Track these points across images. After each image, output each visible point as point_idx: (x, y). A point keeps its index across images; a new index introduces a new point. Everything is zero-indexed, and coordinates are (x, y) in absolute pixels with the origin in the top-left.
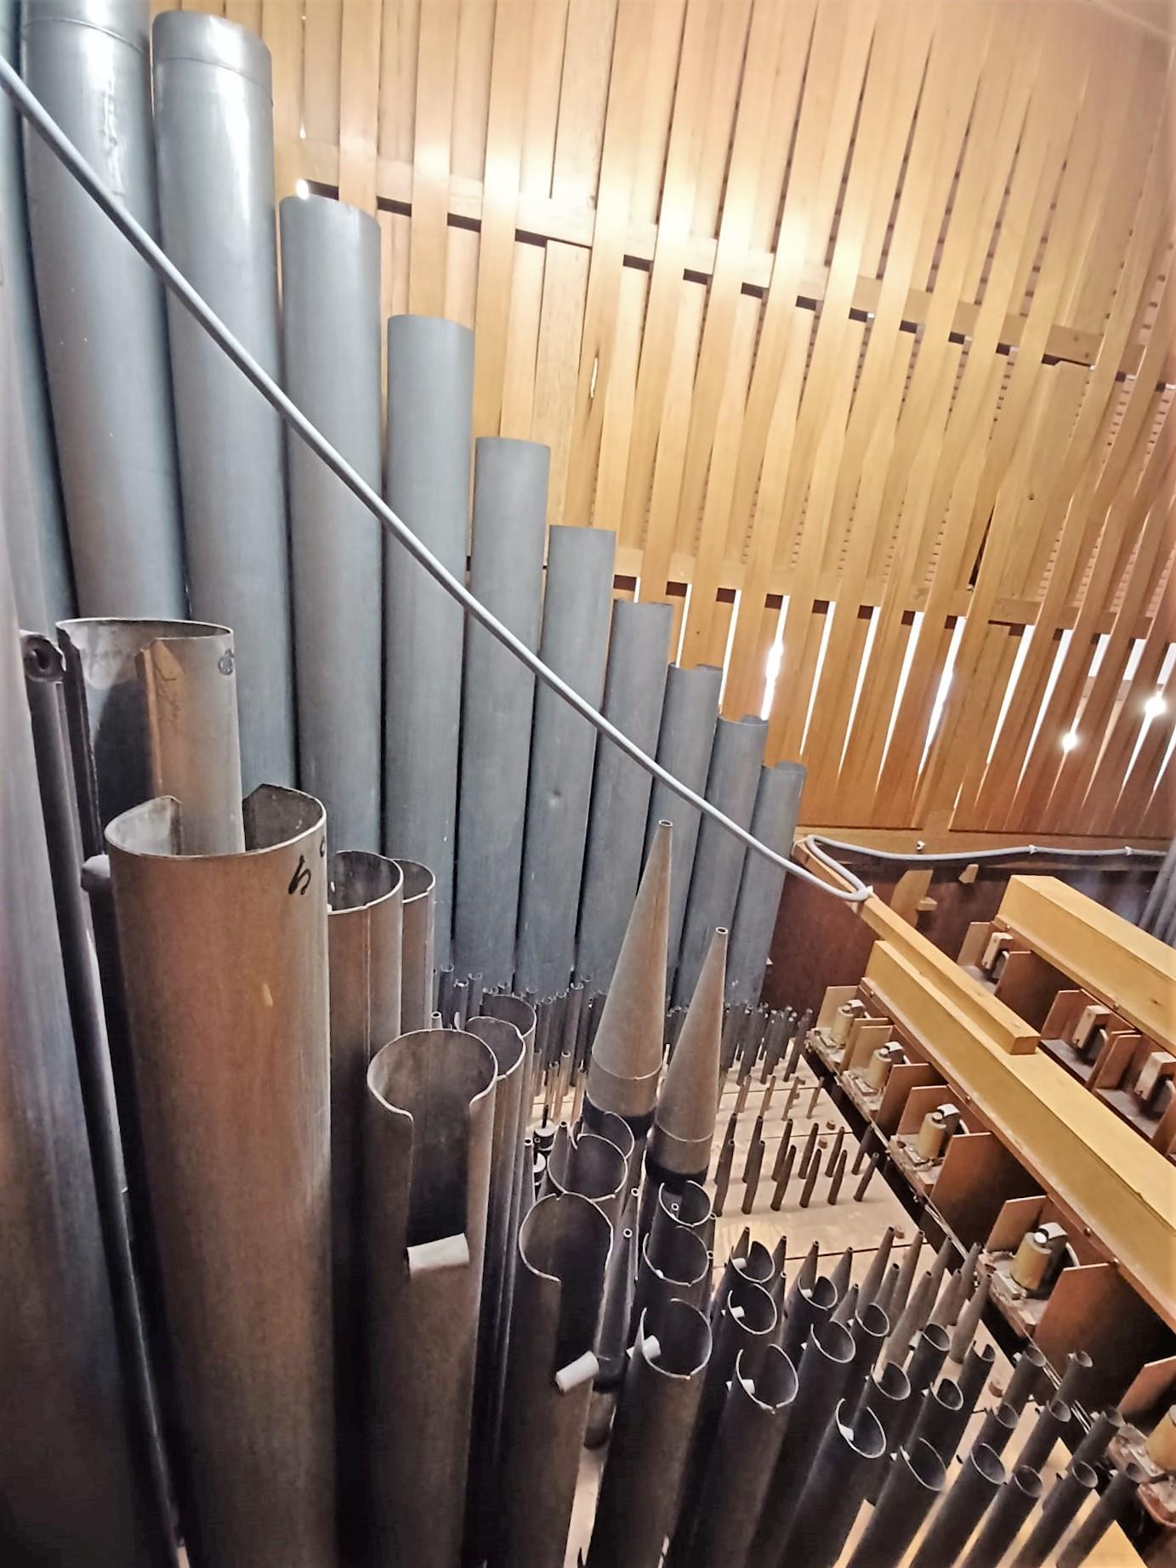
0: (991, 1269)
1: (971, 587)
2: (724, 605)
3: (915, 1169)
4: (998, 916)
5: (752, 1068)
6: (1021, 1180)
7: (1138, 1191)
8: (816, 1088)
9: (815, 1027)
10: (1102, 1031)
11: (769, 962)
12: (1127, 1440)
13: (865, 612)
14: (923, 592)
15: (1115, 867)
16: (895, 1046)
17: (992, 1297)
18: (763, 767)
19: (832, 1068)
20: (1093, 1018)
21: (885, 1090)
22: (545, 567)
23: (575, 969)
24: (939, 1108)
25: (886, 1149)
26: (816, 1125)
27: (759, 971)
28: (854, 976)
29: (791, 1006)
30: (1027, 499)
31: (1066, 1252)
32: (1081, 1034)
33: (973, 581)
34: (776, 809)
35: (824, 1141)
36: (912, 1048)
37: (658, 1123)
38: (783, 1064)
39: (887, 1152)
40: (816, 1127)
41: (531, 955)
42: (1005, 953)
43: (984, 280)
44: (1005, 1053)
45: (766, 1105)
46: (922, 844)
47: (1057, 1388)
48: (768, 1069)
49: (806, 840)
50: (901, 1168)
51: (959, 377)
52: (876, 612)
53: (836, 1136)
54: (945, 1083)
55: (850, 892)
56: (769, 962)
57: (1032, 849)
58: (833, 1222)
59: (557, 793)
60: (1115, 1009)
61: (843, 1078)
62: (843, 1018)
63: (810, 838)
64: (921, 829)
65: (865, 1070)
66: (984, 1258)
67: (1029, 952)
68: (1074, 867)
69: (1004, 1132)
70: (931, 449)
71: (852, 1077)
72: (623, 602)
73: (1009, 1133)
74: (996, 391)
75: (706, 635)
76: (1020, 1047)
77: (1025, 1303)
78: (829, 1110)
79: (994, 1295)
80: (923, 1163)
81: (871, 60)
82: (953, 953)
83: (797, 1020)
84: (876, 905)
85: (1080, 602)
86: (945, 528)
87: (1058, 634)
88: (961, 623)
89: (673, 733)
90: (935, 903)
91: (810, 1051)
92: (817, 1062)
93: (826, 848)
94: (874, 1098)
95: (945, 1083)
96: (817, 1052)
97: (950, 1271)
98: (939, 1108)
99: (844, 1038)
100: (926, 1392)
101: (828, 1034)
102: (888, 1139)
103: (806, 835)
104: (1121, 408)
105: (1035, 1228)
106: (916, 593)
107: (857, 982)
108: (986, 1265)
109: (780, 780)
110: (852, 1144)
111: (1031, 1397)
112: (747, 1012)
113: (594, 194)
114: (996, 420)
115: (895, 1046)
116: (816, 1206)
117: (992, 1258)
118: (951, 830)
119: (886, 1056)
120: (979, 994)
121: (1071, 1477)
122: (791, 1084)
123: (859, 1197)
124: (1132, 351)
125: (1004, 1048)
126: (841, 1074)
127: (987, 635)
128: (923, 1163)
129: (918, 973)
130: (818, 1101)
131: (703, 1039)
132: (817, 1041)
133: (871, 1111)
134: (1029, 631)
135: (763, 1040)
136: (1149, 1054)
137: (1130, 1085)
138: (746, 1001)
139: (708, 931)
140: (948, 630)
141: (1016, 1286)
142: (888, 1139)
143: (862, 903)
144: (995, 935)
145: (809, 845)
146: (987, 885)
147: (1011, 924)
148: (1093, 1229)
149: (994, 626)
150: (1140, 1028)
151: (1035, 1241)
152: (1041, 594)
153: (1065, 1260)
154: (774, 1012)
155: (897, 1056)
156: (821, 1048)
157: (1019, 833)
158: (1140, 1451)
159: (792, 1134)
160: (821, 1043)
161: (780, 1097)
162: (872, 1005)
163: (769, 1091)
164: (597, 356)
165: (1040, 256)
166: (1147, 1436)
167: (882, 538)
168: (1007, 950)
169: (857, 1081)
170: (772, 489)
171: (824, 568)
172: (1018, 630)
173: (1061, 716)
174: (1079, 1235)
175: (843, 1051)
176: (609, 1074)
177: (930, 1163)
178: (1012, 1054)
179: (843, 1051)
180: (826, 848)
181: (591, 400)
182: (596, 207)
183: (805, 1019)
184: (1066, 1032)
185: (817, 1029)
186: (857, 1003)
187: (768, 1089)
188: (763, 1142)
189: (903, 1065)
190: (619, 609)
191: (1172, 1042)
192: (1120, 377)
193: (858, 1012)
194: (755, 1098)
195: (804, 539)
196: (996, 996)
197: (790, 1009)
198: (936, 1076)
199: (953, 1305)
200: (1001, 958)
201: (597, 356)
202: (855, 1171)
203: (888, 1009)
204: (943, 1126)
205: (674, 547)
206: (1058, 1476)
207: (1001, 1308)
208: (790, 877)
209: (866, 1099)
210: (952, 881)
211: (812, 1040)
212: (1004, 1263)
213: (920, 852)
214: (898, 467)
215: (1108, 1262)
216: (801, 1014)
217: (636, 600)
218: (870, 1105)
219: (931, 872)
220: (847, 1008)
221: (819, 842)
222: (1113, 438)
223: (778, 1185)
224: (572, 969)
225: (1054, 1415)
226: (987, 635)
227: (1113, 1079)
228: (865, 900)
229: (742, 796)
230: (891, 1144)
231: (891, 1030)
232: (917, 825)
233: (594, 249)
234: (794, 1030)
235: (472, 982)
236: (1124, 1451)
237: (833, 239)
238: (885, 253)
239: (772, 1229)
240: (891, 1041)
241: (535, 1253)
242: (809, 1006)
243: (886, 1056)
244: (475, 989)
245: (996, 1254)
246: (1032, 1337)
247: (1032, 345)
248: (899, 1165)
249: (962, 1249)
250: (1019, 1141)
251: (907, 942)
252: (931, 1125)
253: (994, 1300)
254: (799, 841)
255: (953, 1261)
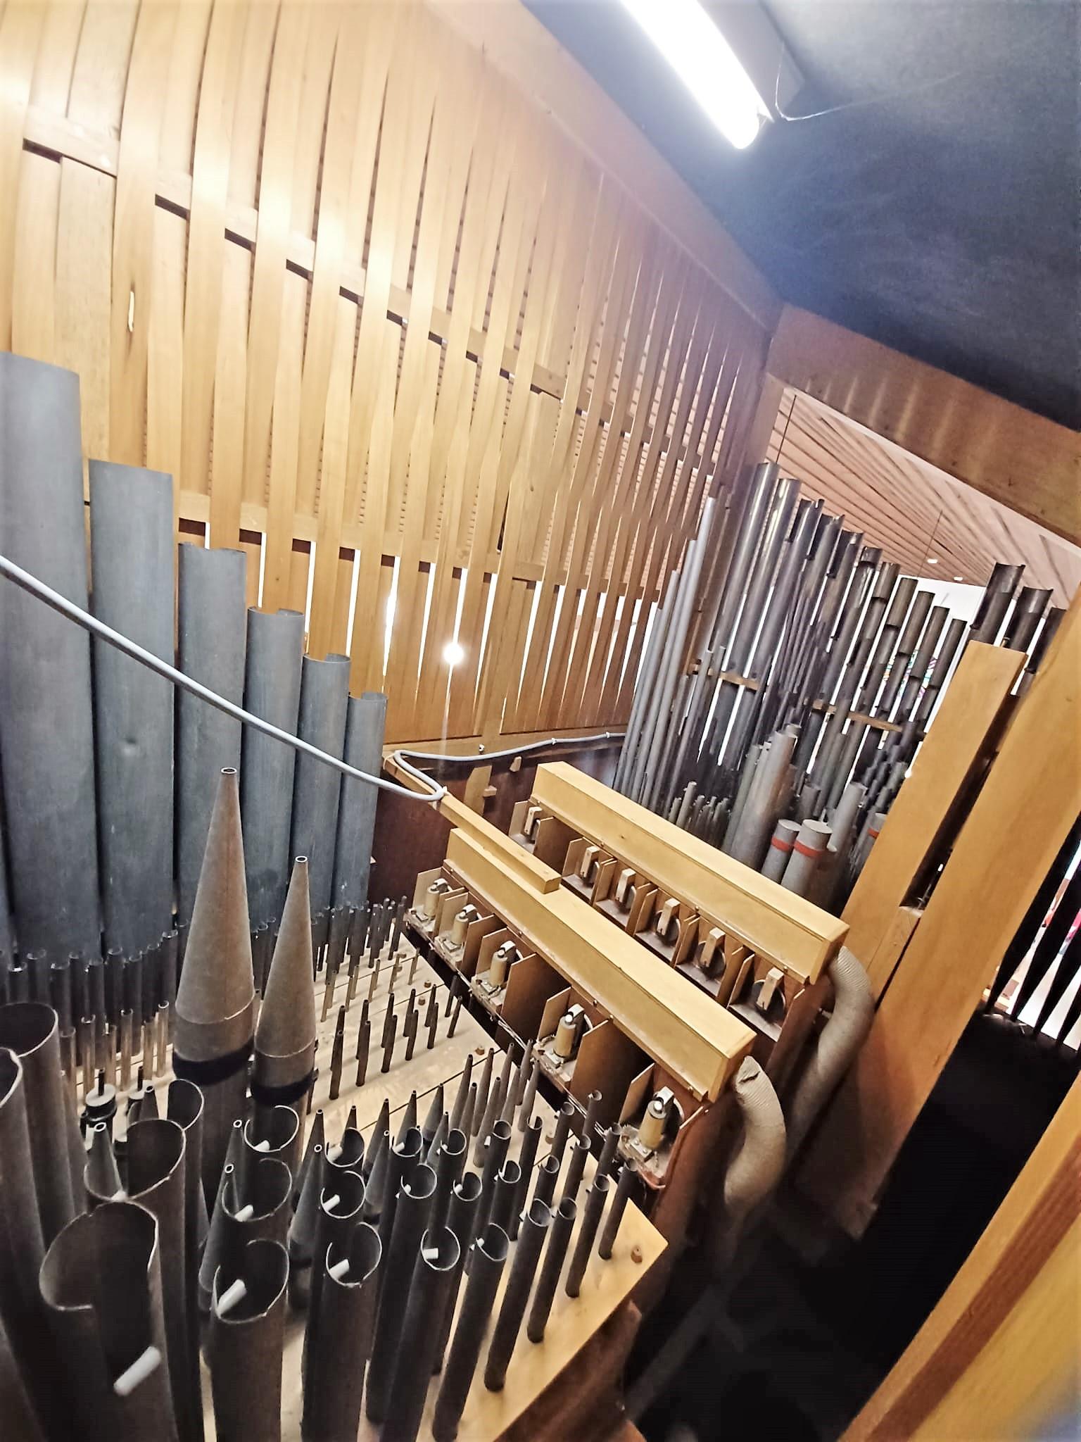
0: (542, 1052)
1: (499, 551)
2: (300, 555)
3: (489, 997)
4: (532, 795)
5: (361, 957)
6: (556, 981)
7: (619, 966)
8: (414, 958)
9: (411, 907)
10: (596, 863)
11: (373, 861)
12: (628, 1138)
13: (424, 567)
14: (466, 553)
15: (601, 747)
16: (470, 908)
17: (543, 1071)
18: (349, 697)
19: (426, 937)
20: (591, 855)
21: (465, 943)
22: (87, 503)
23: (179, 910)
24: (502, 947)
25: (469, 988)
26: (414, 990)
27: (364, 871)
28: (436, 856)
29: (388, 897)
30: (529, 490)
31: (585, 1021)
32: (585, 869)
33: (500, 548)
34: (364, 732)
35: (422, 999)
36: (483, 907)
37: (258, 1049)
38: (388, 945)
39: (470, 991)
40: (414, 992)
41: (122, 912)
42: (538, 821)
43: (487, 313)
44: (540, 893)
45: (374, 986)
46: (482, 747)
47: (585, 1117)
48: (375, 955)
49: (393, 755)
50: (480, 1000)
51: (477, 385)
52: (433, 567)
53: (430, 992)
54: (505, 926)
55: (431, 794)
56: (373, 861)
57: (553, 741)
58: (431, 1064)
59: (132, 741)
60: (602, 847)
61: (435, 944)
62: (431, 894)
63: (397, 753)
64: (480, 736)
65: (451, 932)
66: (537, 1046)
67: (552, 818)
68: (577, 750)
69: (543, 950)
70: (460, 443)
71: (441, 940)
72: (189, 546)
73: (546, 950)
74: (503, 403)
75: (284, 583)
76: (549, 887)
77: (563, 1068)
78: (427, 971)
79: (545, 1070)
80: (494, 991)
81: (387, 97)
82: (504, 827)
83: (395, 907)
84: (451, 802)
85: (567, 567)
86: (477, 509)
87: (557, 588)
88: (495, 578)
89: (259, 674)
90: (495, 789)
91: (409, 928)
92: (415, 936)
93: (411, 760)
94: (459, 952)
95: (505, 926)
96: (414, 927)
97: (516, 1064)
98: (502, 947)
99: (434, 911)
100: (473, 1247)
101: (421, 913)
102: (470, 980)
103: (393, 751)
104: (581, 431)
105: (566, 1013)
106: (461, 554)
107: (441, 864)
108: (539, 1051)
109: (364, 710)
110: (443, 993)
111: (571, 1132)
112: (352, 911)
113: (117, 125)
114: (505, 423)
115: (470, 908)
116: (419, 1054)
117: (542, 1044)
118: (501, 734)
119: (464, 918)
120: (522, 856)
121: (594, 1188)
122: (394, 960)
123: (451, 1035)
124: (584, 394)
125: (538, 889)
126: (433, 940)
127: (512, 587)
128: (494, 991)
129: (482, 848)
130: (417, 968)
131: (296, 955)
132: (413, 919)
133: (456, 962)
134: (539, 585)
135: (369, 929)
136: (620, 873)
137: (613, 896)
138: (349, 903)
139: (313, 849)
140: (486, 584)
141: (557, 1058)
142: (470, 980)
143: (439, 801)
144: (531, 809)
145: (396, 759)
146: (527, 770)
147: (540, 799)
148: (599, 1001)
149: (516, 581)
150: (617, 857)
151: (566, 1022)
152: (544, 560)
153: (584, 1027)
154: (375, 906)
155: (472, 916)
156: (417, 923)
157: (544, 731)
158: (636, 1142)
159: (395, 1004)
160: (417, 919)
161: (385, 976)
162: (453, 880)
163: (375, 974)
164: (133, 289)
165: (524, 305)
166: (638, 1129)
167: (431, 509)
168: (539, 819)
169: (445, 942)
170: (334, 454)
171: (387, 527)
172: (531, 585)
173: (438, 634)
174: (592, 1008)
175: (434, 922)
176: (196, 1024)
177: (500, 988)
178: (545, 893)
179: (434, 922)
180: (411, 760)
181: (130, 334)
182: (119, 139)
183: (401, 905)
184: (577, 870)
185: (413, 909)
186: (441, 881)
187: (374, 972)
188: (369, 1022)
189: (478, 921)
190: (186, 555)
191: (867, 340)
192: (579, 412)
193: (443, 888)
194: (363, 983)
195: (367, 504)
196: (534, 854)
197: (388, 900)
198: (499, 923)
199: (519, 1086)
200: (536, 825)
201: (133, 289)
202: (447, 1015)
203: (465, 881)
204: (505, 959)
205: (243, 497)
206: (587, 1191)
207: (549, 1076)
208: (382, 791)
209: (452, 954)
210: (505, 772)
211: (408, 918)
212: (550, 1044)
213: (481, 753)
214: (439, 452)
215: (608, 1019)
216: (398, 901)
217: (207, 546)
218: (455, 960)
219: (490, 767)
220: (434, 887)
221: (405, 755)
222: (578, 451)
223: (386, 1051)
224: (174, 912)
225: (583, 1148)
226: (512, 587)
227: (603, 894)
228: (441, 799)
229: (332, 728)
230: (472, 985)
231: (467, 898)
232: (479, 732)
233: (118, 178)
234: (394, 913)
235: (31, 963)
236: (627, 1146)
237: (367, 242)
238: (412, 268)
239: (383, 1088)
240: (467, 904)
241: (67, 1292)
242: (405, 893)
243: (464, 918)
244: (38, 969)
245: (545, 1039)
246: (569, 1090)
247: (523, 376)
248: (478, 997)
249: (522, 1044)
250: (553, 954)
251: (473, 826)
252: (498, 960)
253: (546, 1073)
254: (388, 757)
255: (517, 1056)
